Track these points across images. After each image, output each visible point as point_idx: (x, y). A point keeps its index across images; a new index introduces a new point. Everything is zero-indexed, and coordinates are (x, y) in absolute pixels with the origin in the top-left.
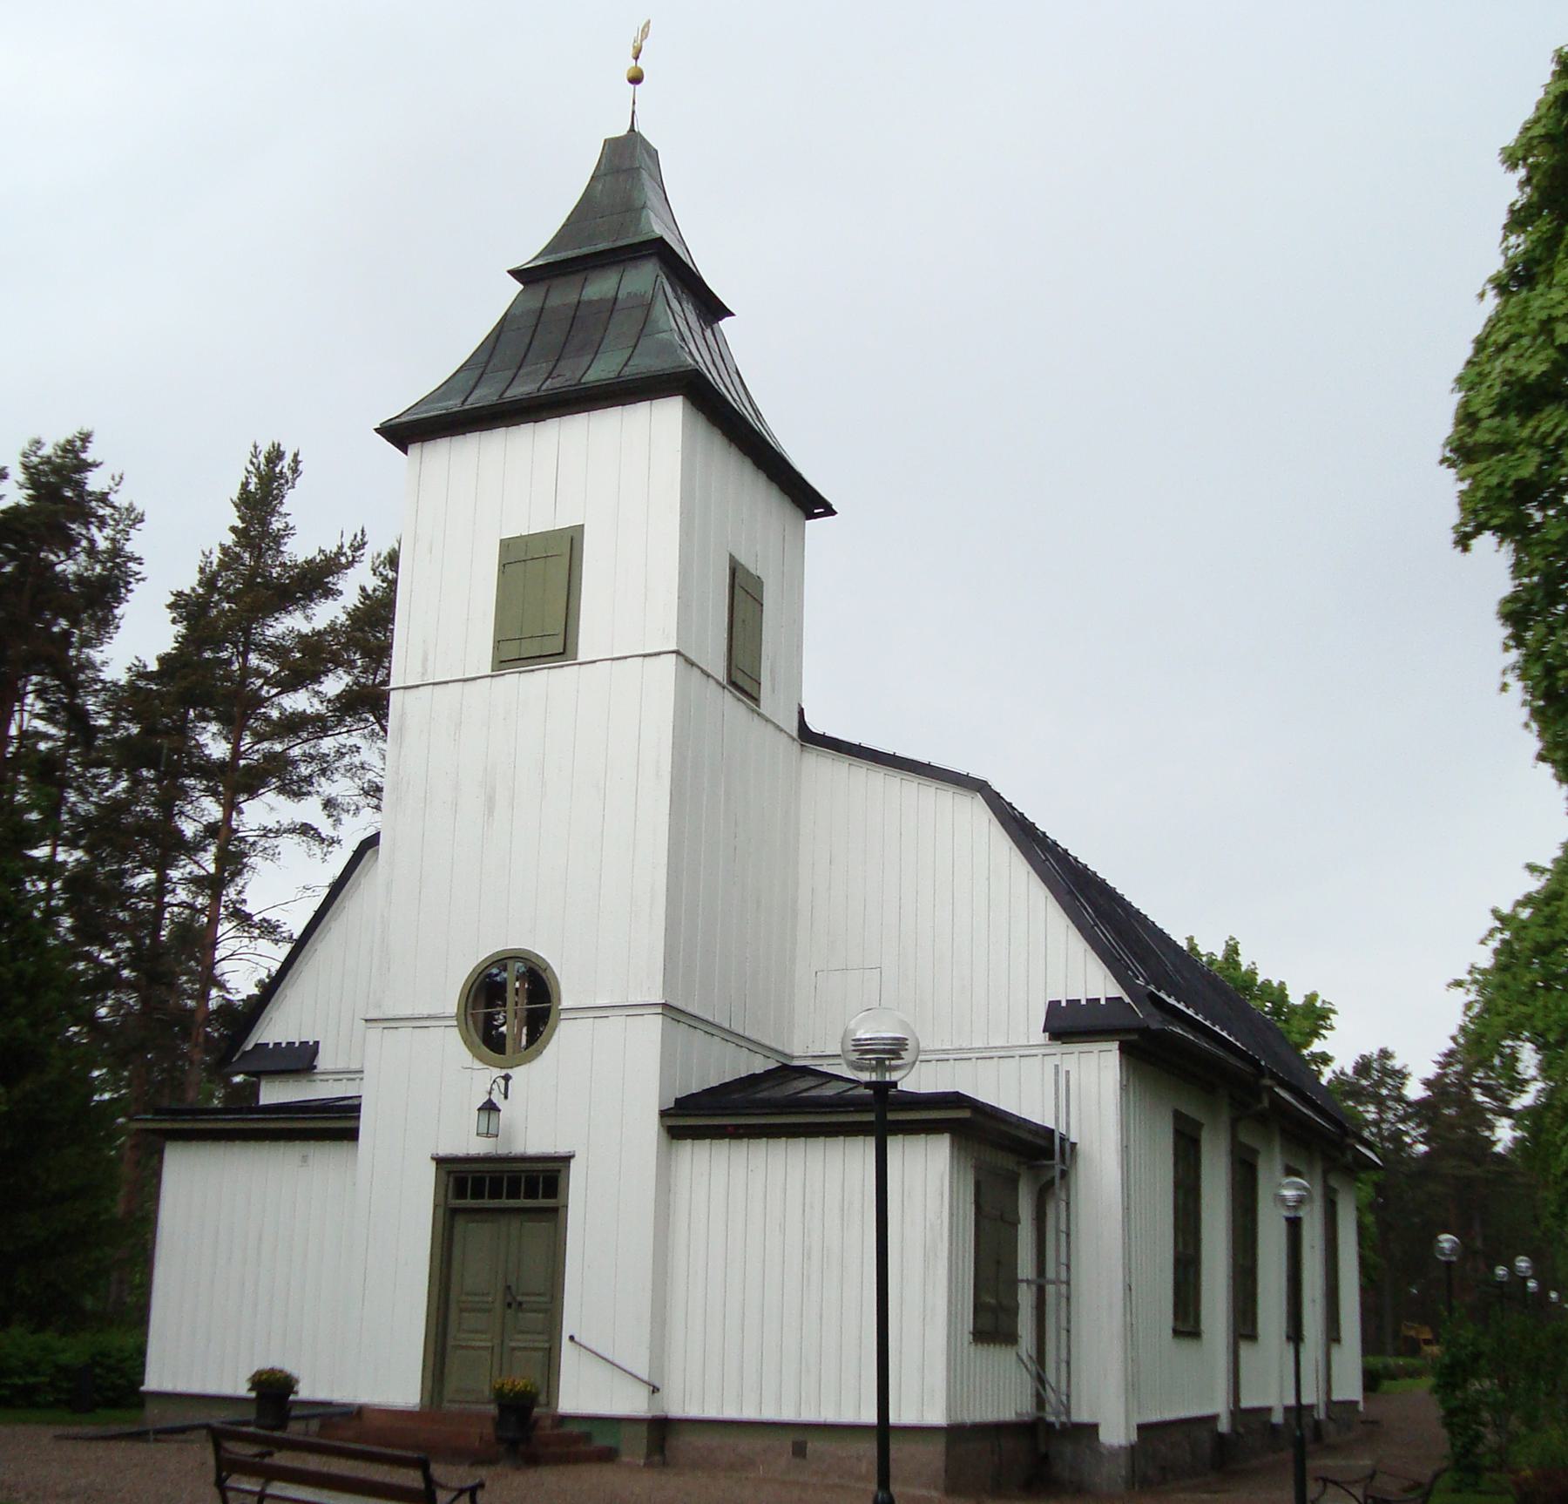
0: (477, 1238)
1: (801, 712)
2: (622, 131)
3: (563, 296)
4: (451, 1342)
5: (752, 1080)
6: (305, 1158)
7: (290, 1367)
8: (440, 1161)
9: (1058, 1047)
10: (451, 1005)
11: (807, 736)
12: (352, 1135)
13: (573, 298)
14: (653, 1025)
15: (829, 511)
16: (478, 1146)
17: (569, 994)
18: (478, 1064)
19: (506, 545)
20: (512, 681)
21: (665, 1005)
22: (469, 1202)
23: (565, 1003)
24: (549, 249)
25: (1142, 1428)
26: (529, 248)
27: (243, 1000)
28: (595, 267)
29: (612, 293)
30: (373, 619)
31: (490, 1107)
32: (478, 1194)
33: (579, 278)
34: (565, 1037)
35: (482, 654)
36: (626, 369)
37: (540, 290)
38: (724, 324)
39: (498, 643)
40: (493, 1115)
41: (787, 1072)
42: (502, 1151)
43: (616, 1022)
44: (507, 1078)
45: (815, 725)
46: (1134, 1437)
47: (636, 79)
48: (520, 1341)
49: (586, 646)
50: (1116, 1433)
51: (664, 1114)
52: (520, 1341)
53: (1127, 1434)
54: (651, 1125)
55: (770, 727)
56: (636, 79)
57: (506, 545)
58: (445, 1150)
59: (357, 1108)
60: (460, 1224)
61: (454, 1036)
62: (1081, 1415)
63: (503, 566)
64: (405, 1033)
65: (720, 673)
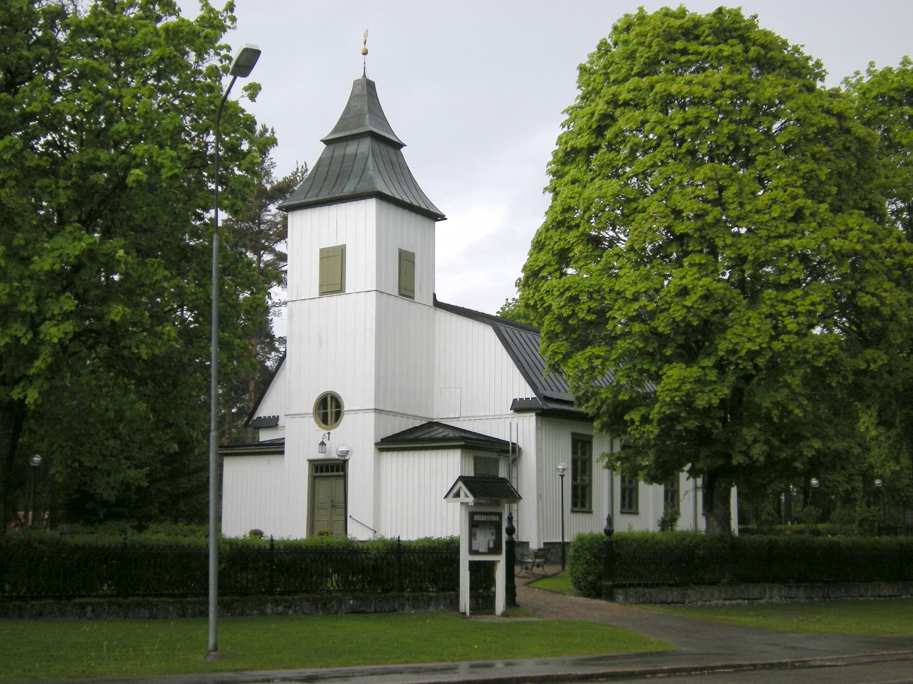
0: (322, 485)
1: (435, 295)
2: (360, 76)
3: (339, 151)
4: (316, 519)
5: (415, 429)
6: (269, 461)
7: (262, 529)
8: (310, 461)
9: (517, 415)
10: (311, 410)
11: (438, 305)
12: (282, 453)
13: (342, 153)
14: (372, 416)
15: (443, 218)
16: (321, 456)
17: (346, 406)
18: (320, 429)
19: (322, 251)
20: (326, 299)
21: (375, 409)
22: (319, 474)
23: (346, 408)
24: (335, 131)
25: (545, 544)
26: (327, 128)
27: (48, 177)
28: (350, 139)
29: (354, 152)
30: (280, 609)
31: (323, 444)
32: (322, 471)
33: (345, 143)
34: (346, 419)
35: (316, 292)
36: (359, 186)
37: (332, 147)
38: (403, 150)
39: (320, 286)
40: (324, 446)
41: (431, 424)
42: (328, 457)
43: (361, 414)
44: (329, 433)
45: (439, 299)
46: (542, 546)
47: (365, 53)
48: (335, 518)
49: (349, 286)
50: (534, 546)
51: (376, 444)
52: (335, 518)
53: (539, 544)
54: (371, 448)
55: (420, 305)
56: (365, 53)
57: (322, 251)
58: (311, 458)
59: (283, 444)
60: (317, 480)
61: (312, 419)
62: (525, 540)
63: (321, 259)
64: (297, 419)
65: (397, 294)
